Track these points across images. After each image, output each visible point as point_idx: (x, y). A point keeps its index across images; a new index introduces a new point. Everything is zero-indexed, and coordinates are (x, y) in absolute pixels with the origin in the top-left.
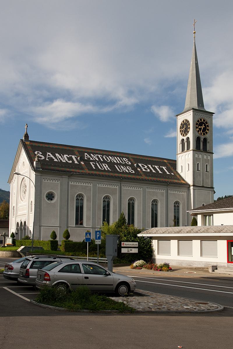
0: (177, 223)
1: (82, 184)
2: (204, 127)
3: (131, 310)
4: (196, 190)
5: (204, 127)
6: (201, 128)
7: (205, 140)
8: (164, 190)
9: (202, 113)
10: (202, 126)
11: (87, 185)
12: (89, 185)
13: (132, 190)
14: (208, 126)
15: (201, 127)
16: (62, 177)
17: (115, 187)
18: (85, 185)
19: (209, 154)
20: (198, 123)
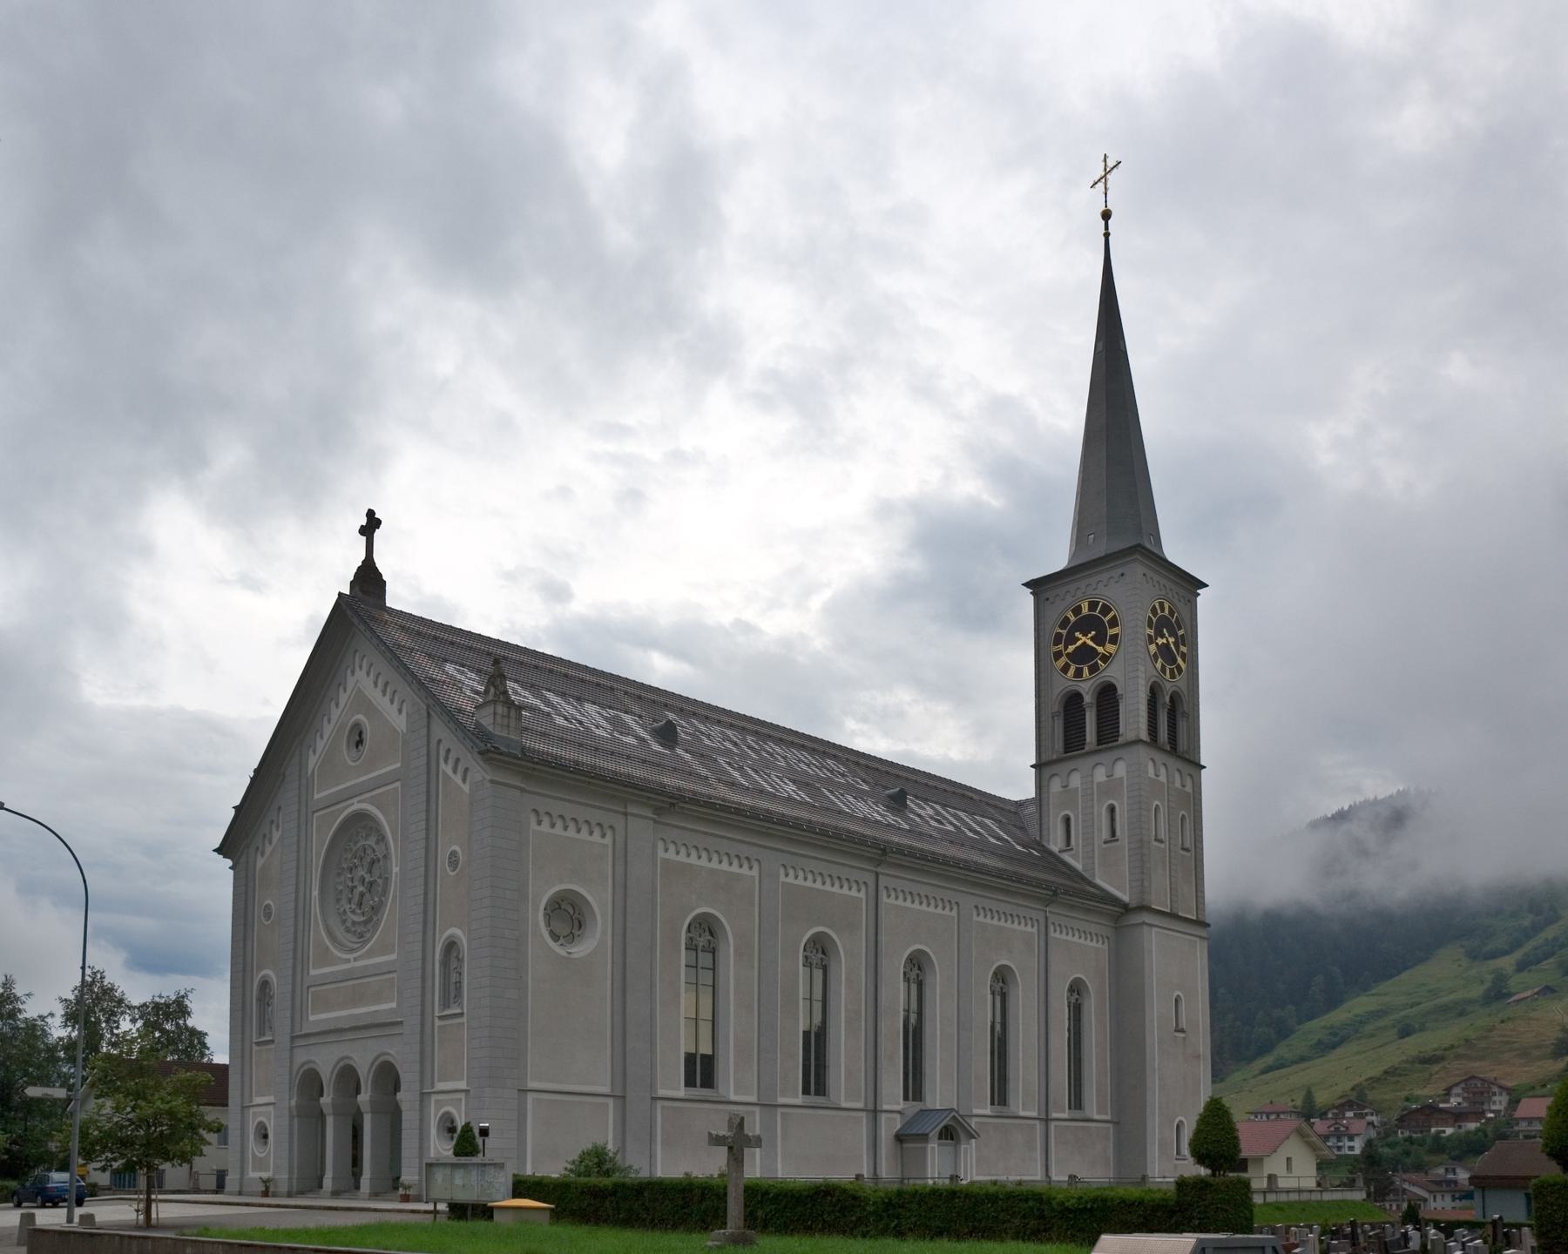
0: (686, 966)
1: (714, 865)
2: (1077, 634)
3: (102, 1071)
4: (1154, 929)
5: (1077, 634)
6: (1079, 639)
7: (1175, 699)
8: (609, 833)
9: (1182, 583)
10: (1085, 642)
11: (735, 868)
12: (745, 870)
13: (811, 889)
14: (1062, 626)
15: (1090, 643)
16: (626, 814)
17: (854, 893)
18: (725, 866)
19: (1180, 765)
20: (1154, 620)
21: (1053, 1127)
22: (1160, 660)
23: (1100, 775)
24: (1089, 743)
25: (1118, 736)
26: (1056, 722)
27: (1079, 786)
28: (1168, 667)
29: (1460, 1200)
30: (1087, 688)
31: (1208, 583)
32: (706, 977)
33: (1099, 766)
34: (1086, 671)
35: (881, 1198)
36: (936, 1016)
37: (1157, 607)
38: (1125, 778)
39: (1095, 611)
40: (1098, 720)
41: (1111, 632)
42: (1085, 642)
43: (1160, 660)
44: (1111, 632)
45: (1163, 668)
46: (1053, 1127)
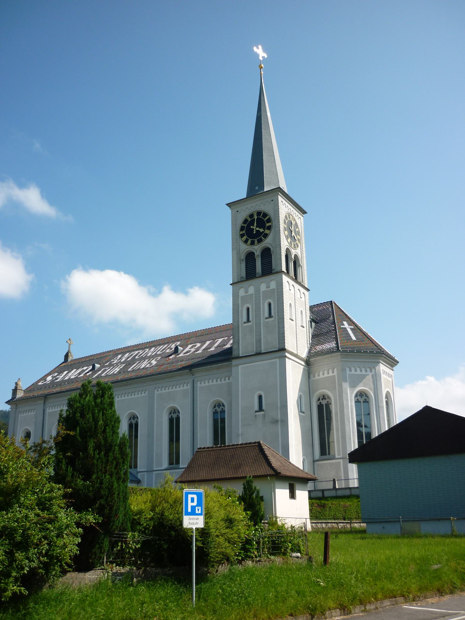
10: (254, 229)
21: (341, 454)
22: (289, 239)
23: (263, 287)
24: (258, 273)
25: (256, 275)
26: (242, 264)
27: (254, 293)
28: (293, 243)
29: (60, 413)
30: (257, 249)
31: (306, 211)
32: (364, 430)
33: (273, 281)
34: (249, 242)
35: (113, 491)
36: (239, 407)
37: (287, 216)
38: (276, 289)
39: (260, 216)
40: (246, 268)
41: (268, 225)
42: (256, 227)
43: (289, 239)
44: (268, 225)
45: (291, 243)
46: (341, 454)
